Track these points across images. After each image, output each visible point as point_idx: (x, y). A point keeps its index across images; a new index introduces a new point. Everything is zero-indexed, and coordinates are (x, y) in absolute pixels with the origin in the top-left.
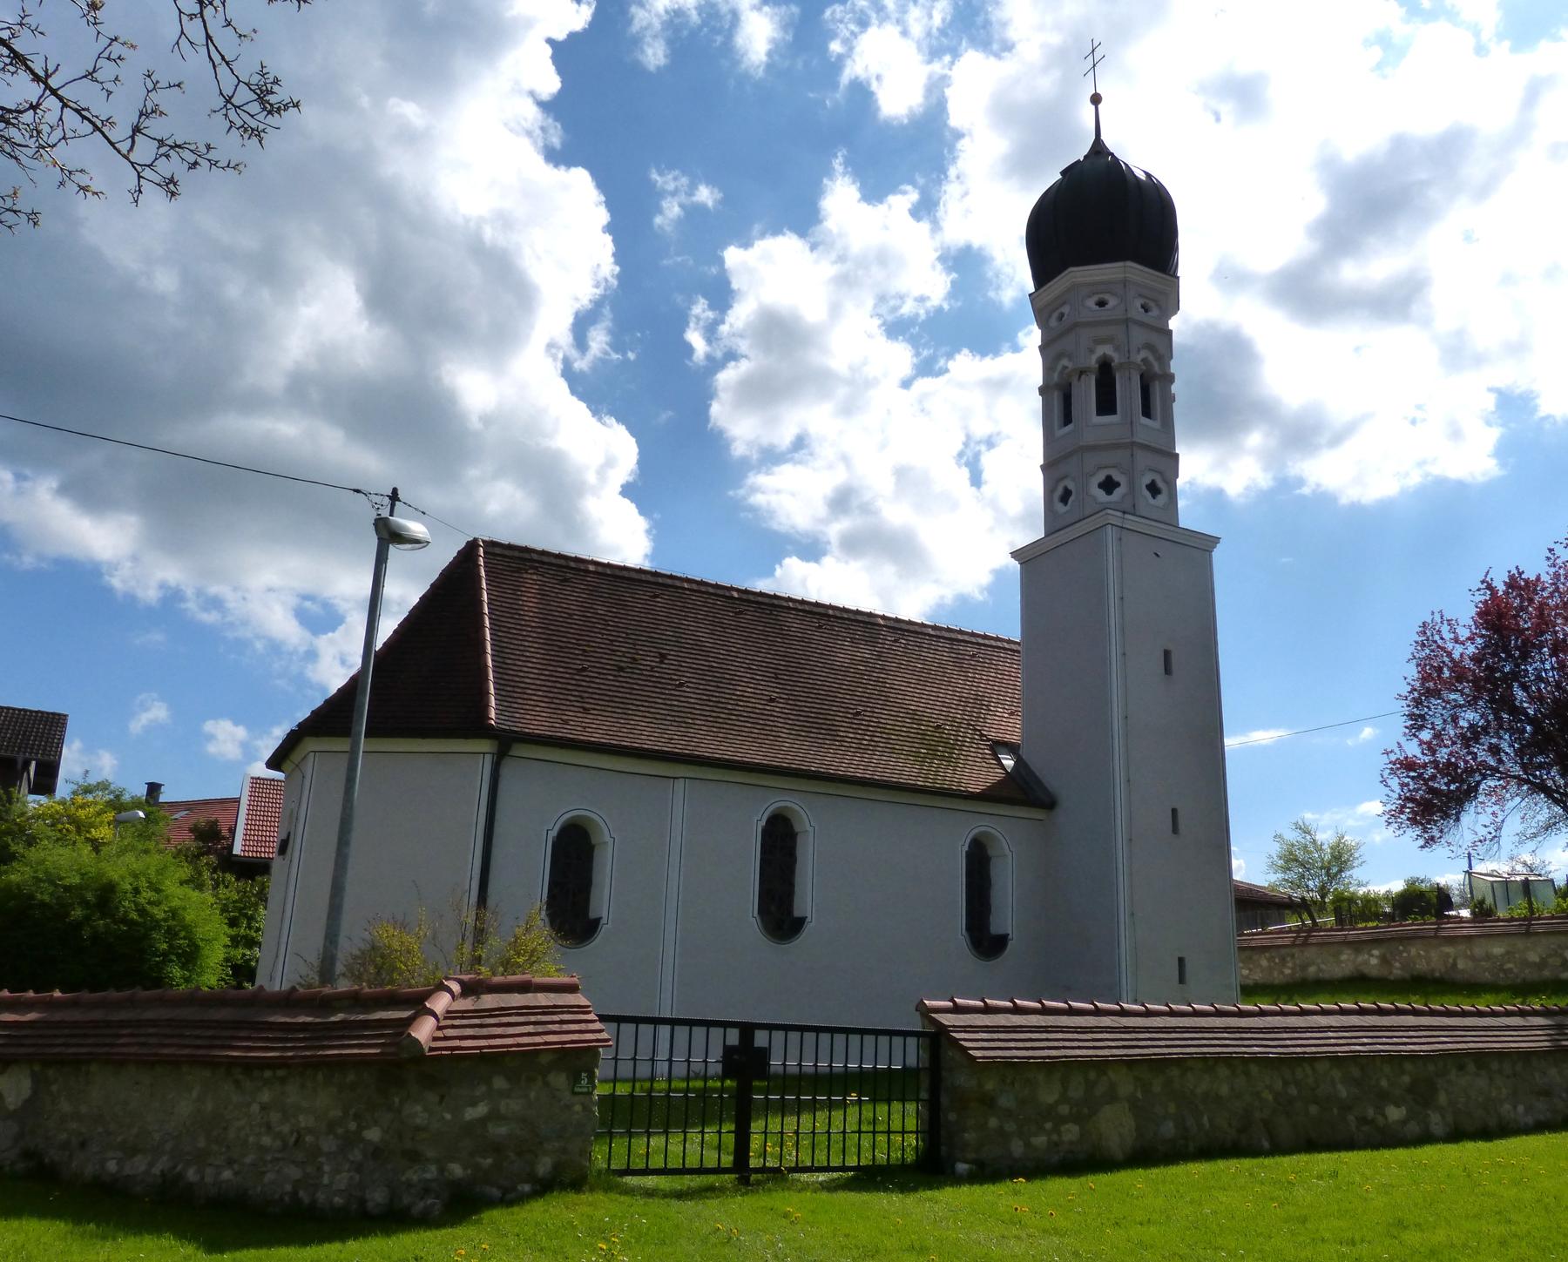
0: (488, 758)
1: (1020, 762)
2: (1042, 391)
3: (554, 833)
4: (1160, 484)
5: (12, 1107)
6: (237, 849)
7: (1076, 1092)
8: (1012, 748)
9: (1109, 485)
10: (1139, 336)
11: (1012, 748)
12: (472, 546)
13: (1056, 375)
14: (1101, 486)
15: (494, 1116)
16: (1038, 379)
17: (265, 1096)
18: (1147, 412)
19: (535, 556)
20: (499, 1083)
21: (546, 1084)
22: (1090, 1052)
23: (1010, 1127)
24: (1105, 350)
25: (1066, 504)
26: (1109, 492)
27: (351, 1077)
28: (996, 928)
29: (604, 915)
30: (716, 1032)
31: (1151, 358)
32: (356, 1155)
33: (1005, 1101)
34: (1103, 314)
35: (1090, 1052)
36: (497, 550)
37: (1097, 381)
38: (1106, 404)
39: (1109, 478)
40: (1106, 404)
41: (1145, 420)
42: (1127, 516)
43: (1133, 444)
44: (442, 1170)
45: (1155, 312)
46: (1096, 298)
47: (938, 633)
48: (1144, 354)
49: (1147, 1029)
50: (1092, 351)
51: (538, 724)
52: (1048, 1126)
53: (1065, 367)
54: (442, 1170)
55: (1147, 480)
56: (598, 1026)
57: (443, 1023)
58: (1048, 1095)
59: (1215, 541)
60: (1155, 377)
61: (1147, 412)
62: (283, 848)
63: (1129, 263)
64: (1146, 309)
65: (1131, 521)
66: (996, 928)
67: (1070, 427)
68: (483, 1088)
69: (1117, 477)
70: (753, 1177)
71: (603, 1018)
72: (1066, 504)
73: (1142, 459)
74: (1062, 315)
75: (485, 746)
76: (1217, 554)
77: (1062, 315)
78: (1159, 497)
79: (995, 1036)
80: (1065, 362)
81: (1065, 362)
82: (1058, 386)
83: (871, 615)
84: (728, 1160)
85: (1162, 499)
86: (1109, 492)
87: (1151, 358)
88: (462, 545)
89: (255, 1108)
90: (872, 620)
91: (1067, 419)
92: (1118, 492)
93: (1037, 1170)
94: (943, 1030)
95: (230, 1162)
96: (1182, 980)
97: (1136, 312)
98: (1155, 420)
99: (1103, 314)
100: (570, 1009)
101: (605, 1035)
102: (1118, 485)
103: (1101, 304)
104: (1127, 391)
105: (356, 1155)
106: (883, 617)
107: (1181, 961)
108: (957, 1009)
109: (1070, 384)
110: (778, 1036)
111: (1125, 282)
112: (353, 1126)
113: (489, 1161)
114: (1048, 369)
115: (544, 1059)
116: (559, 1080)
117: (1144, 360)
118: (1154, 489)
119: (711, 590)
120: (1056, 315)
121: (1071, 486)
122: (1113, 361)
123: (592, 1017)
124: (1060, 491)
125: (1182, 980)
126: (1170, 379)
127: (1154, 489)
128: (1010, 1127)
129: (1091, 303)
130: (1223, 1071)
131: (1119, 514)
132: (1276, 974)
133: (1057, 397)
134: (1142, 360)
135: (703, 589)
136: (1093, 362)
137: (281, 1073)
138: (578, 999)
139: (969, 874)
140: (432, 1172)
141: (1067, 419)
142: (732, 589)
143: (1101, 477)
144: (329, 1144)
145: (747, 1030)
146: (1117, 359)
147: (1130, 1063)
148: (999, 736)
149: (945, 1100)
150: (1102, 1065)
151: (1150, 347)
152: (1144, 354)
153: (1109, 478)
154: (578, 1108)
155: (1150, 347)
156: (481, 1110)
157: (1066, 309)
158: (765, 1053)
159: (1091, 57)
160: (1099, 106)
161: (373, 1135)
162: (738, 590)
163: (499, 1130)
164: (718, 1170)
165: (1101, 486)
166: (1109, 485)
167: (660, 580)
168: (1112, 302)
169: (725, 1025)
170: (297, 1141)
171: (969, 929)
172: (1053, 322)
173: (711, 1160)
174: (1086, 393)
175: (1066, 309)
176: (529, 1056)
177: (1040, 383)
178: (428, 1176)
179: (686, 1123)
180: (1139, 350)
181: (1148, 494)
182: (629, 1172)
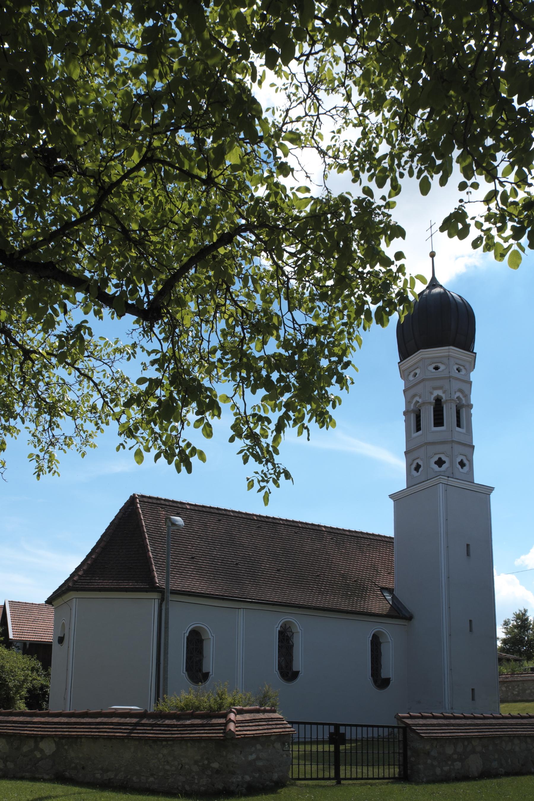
0: (156, 601)
1: (394, 598)
2: (405, 413)
3: (187, 634)
4: (465, 461)
5: (48, 754)
6: (11, 636)
7: (460, 749)
8: (391, 591)
9: (440, 463)
10: (456, 385)
11: (391, 591)
12: (133, 498)
13: (412, 405)
14: (436, 463)
15: (258, 758)
16: (403, 407)
17: (165, 751)
18: (459, 425)
19: (162, 502)
20: (259, 747)
21: (274, 747)
22: (448, 735)
23: (435, 763)
24: (439, 393)
25: (418, 472)
26: (440, 466)
27: (203, 744)
28: (384, 675)
29: (211, 671)
30: (326, 727)
31: (461, 396)
32: (209, 772)
33: (434, 753)
34: (437, 374)
35: (448, 735)
36: (145, 500)
37: (434, 408)
38: (439, 421)
39: (440, 459)
40: (439, 421)
41: (458, 429)
42: (450, 479)
43: (453, 441)
44: (243, 778)
45: (463, 372)
46: (434, 365)
47: (351, 534)
48: (458, 394)
49: (485, 725)
50: (431, 393)
51: (176, 584)
52: (450, 763)
53: (418, 402)
54: (243, 778)
55: (459, 460)
56: (289, 726)
57: (237, 725)
58: (449, 750)
59: (492, 489)
60: (463, 406)
61: (459, 425)
62: (61, 640)
63: (452, 347)
64: (459, 370)
65: (452, 481)
66: (384, 675)
67: (420, 433)
68: (253, 749)
69: (444, 458)
70: (343, 782)
71: (289, 723)
72: (418, 472)
73: (458, 448)
74: (416, 374)
75: (156, 595)
76: (493, 496)
77: (415, 374)
78: (465, 468)
79: (429, 728)
80: (417, 399)
81: (417, 399)
82: (413, 411)
83: (319, 526)
84: (333, 775)
85: (466, 469)
86: (440, 466)
87: (461, 396)
88: (128, 498)
89: (160, 756)
90: (320, 528)
91: (418, 428)
92: (444, 466)
93: (446, 779)
94: (408, 725)
95: (152, 775)
96: (473, 699)
97: (455, 373)
98: (463, 428)
99: (437, 374)
100: (272, 719)
101: (292, 729)
102: (444, 462)
103: (436, 368)
104: (449, 414)
105: (209, 772)
106: (325, 527)
107: (473, 690)
108: (411, 717)
109: (420, 410)
110: (348, 728)
111: (449, 357)
112: (206, 762)
113: (258, 775)
114: (408, 403)
115: (273, 738)
116: (278, 745)
117: (458, 398)
118: (462, 464)
119: (244, 516)
120: (412, 373)
121: (420, 463)
122: (442, 398)
123: (285, 722)
124: (414, 466)
125: (473, 699)
126: (471, 406)
127: (462, 464)
128: (435, 763)
129: (431, 368)
130: (516, 741)
131: (446, 478)
132: (509, 694)
133: (413, 417)
134: (457, 398)
135: (240, 516)
136: (432, 399)
137: (170, 743)
138: (276, 715)
139: (372, 651)
140: (239, 779)
141: (418, 428)
142: (253, 515)
143: (436, 458)
144: (195, 768)
145: (337, 726)
146: (444, 397)
147: (481, 738)
148: (384, 585)
149: (409, 753)
150: (469, 739)
151: (461, 391)
152: (458, 394)
153: (440, 459)
154: (285, 756)
155: (461, 391)
156: (254, 756)
157: (418, 371)
158: (344, 735)
159: (313, 51)
160: (435, 258)
161: (215, 765)
162: (256, 516)
163: (260, 764)
164: (329, 779)
165: (436, 463)
166: (440, 463)
167: (220, 512)
168: (442, 367)
169: (329, 724)
170: (181, 768)
171: (372, 675)
172: (411, 378)
173: (327, 775)
174: (428, 416)
175: (418, 371)
176: (268, 737)
177: (404, 409)
178: (238, 780)
179: (317, 762)
180: (455, 392)
181: (459, 467)
182: (299, 779)
